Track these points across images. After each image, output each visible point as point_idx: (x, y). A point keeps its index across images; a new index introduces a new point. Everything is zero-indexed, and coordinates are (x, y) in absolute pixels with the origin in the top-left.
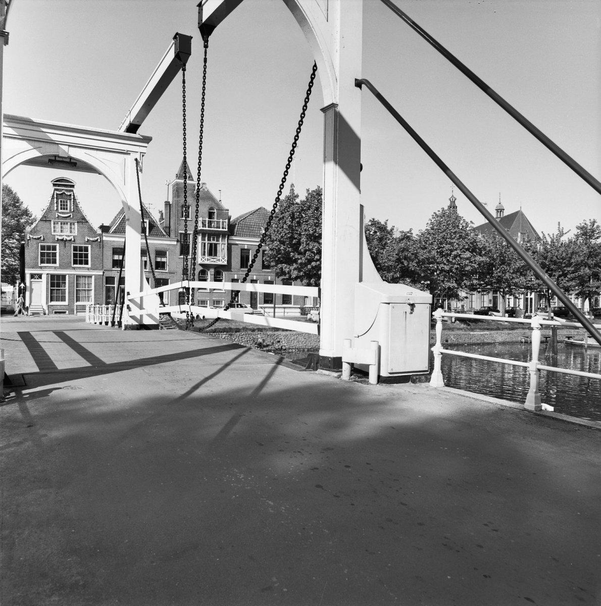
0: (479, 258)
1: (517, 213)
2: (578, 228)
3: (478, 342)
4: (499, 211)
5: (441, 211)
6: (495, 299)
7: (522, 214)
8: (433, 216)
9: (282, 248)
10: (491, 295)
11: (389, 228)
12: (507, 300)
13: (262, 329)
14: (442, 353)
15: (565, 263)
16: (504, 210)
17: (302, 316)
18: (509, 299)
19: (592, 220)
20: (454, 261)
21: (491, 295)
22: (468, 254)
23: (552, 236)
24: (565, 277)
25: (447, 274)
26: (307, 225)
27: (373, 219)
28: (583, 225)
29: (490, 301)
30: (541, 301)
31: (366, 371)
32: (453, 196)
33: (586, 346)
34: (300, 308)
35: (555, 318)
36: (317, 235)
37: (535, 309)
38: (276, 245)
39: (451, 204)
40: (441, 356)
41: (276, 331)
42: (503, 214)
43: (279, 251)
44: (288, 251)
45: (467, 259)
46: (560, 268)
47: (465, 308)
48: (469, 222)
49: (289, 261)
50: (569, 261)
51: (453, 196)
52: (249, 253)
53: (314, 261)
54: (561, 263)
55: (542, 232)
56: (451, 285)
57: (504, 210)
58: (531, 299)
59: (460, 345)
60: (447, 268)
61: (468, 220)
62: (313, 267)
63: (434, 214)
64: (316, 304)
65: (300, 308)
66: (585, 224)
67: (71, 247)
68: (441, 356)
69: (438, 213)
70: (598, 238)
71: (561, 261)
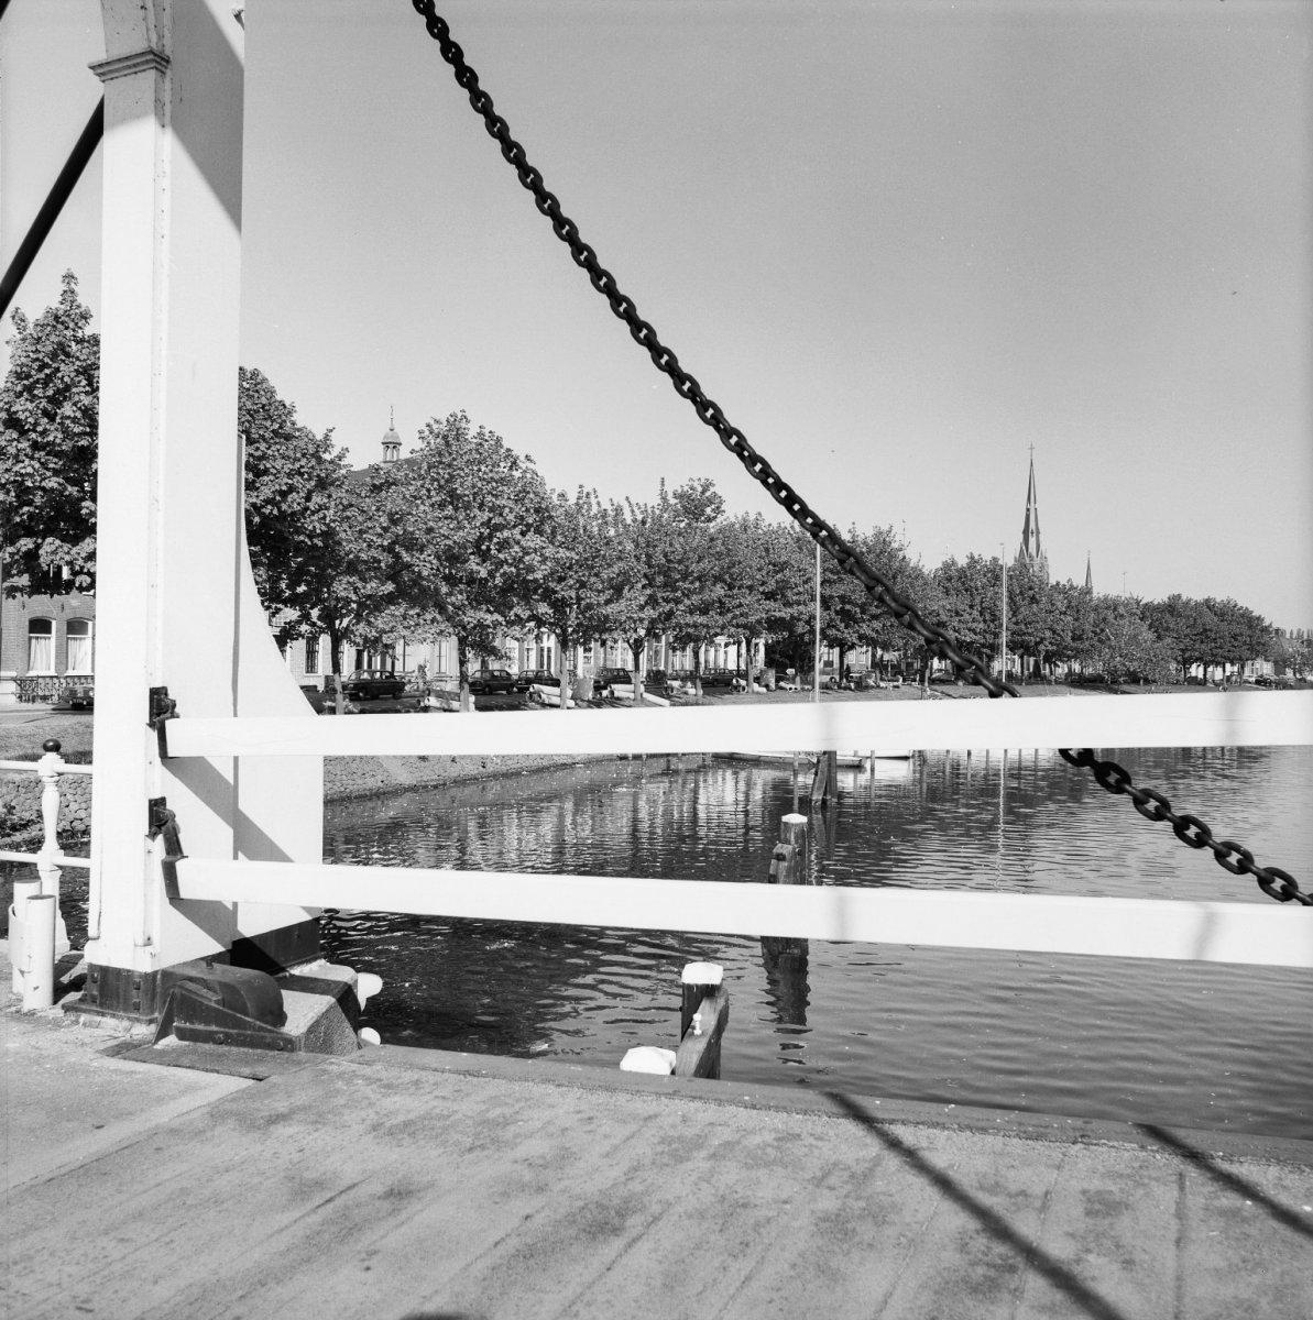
14: (60, 867)
16: (400, 444)
17: (25, 706)
18: (528, 649)
19: (703, 481)
20: (501, 556)
22: (532, 541)
28: (686, 488)
31: (228, 955)
33: (796, 764)
34: (14, 679)
35: (646, 695)
40: (60, 872)
42: (398, 455)
47: (428, 673)
48: (522, 458)
57: (400, 444)
58: (549, 650)
61: (520, 452)
63: (426, 429)
64: (63, 667)
65: (14, 679)
68: (60, 872)
69: (435, 426)
70: (709, 520)
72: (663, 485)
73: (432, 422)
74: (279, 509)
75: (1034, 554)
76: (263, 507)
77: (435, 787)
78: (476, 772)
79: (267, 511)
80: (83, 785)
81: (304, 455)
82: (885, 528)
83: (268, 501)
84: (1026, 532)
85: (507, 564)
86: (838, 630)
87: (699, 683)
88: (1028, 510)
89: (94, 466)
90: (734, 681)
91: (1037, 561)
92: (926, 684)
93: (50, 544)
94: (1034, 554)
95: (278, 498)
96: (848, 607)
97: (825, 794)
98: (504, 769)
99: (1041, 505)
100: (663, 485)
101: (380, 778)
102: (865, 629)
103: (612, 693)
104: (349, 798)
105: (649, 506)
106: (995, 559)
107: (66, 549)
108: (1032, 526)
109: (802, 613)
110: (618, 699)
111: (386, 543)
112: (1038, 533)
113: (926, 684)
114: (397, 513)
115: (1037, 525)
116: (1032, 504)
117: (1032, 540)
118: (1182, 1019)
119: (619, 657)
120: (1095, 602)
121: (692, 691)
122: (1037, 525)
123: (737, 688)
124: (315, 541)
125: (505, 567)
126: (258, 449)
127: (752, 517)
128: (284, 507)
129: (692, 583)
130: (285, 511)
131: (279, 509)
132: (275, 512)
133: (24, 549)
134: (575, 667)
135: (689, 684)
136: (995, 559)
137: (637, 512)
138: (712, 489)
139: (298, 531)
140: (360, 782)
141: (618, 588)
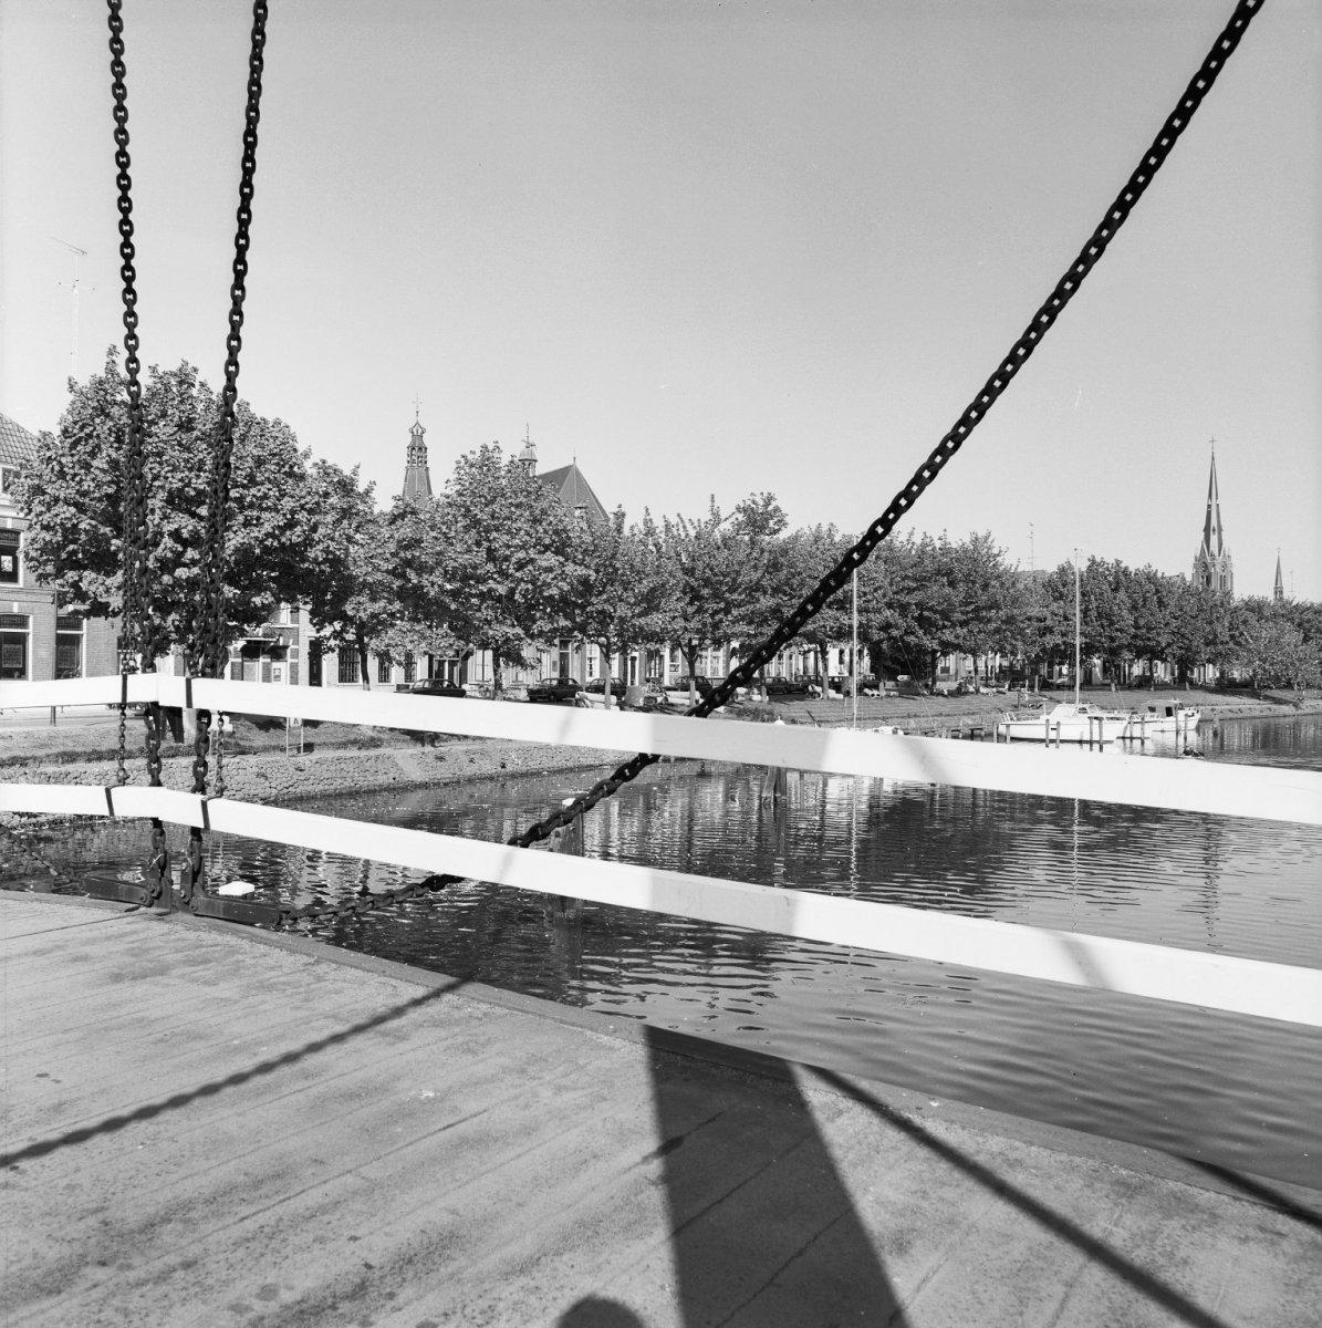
0: (570, 568)
1: (565, 472)
2: (394, 498)
3: (570, 764)
4: (527, 463)
5: (478, 454)
6: (563, 657)
7: (578, 474)
8: (459, 462)
9: (82, 526)
10: (555, 653)
11: (361, 488)
12: (588, 662)
13: (27, 758)
15: (727, 584)
16: (536, 461)
19: (765, 495)
20: (518, 574)
21: (555, 653)
22: (549, 559)
23: (696, 524)
24: (726, 615)
25: (506, 604)
26: (160, 464)
27: (324, 462)
28: (749, 502)
29: (554, 663)
30: (653, 663)
32: (417, 423)
36: (193, 493)
37: (640, 680)
38: (68, 515)
39: (414, 441)
41: (68, 762)
43: (71, 532)
44: (105, 534)
45: (549, 570)
46: (717, 596)
49: (103, 562)
50: (734, 580)
51: (417, 423)
52: (17, 540)
53: (185, 565)
54: (721, 583)
55: (679, 515)
56: (511, 631)
57: (536, 461)
59: (532, 774)
60: (502, 590)
62: (177, 583)
66: (754, 502)
67: (25, 581)
69: (470, 457)
70: (776, 532)
71: (722, 578)
72: (713, 501)
73: (468, 454)
74: (279, 541)
75: (1216, 553)
76: (266, 540)
77: (446, 784)
78: (494, 771)
79: (268, 543)
80: (107, 777)
81: (309, 493)
82: (982, 534)
83: (268, 535)
84: (1207, 530)
85: (525, 581)
86: (917, 637)
87: (764, 689)
88: (1209, 506)
89: (308, 467)
90: (810, 688)
91: (1219, 560)
92: (1036, 690)
93: (89, 575)
94: (1216, 553)
95: (277, 532)
96: (926, 613)
97: (775, 792)
98: (524, 769)
99: (1224, 501)
100: (713, 501)
101: (391, 775)
102: (948, 636)
103: (666, 699)
104: (357, 792)
105: (703, 521)
106: (1118, 563)
107: (100, 581)
108: (1214, 523)
109: (871, 620)
110: (672, 705)
111: (390, 568)
112: (1220, 530)
113: (1036, 690)
114: (404, 540)
115: (1219, 522)
116: (1214, 500)
117: (1214, 539)
118: (1224, 1029)
119: (709, 664)
120: (1233, 605)
121: (756, 697)
122: (1219, 522)
123: (814, 695)
124: (323, 567)
125: (523, 584)
126: (259, 490)
127: (825, 528)
128: (283, 540)
129: (740, 594)
130: (284, 544)
131: (279, 541)
132: (275, 544)
133: (70, 581)
134: (661, 675)
135: (756, 691)
136: (1118, 563)
137: (689, 527)
138: (774, 504)
139: (304, 560)
140: (371, 779)
141: (650, 602)
